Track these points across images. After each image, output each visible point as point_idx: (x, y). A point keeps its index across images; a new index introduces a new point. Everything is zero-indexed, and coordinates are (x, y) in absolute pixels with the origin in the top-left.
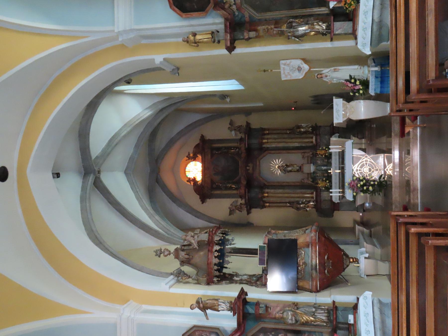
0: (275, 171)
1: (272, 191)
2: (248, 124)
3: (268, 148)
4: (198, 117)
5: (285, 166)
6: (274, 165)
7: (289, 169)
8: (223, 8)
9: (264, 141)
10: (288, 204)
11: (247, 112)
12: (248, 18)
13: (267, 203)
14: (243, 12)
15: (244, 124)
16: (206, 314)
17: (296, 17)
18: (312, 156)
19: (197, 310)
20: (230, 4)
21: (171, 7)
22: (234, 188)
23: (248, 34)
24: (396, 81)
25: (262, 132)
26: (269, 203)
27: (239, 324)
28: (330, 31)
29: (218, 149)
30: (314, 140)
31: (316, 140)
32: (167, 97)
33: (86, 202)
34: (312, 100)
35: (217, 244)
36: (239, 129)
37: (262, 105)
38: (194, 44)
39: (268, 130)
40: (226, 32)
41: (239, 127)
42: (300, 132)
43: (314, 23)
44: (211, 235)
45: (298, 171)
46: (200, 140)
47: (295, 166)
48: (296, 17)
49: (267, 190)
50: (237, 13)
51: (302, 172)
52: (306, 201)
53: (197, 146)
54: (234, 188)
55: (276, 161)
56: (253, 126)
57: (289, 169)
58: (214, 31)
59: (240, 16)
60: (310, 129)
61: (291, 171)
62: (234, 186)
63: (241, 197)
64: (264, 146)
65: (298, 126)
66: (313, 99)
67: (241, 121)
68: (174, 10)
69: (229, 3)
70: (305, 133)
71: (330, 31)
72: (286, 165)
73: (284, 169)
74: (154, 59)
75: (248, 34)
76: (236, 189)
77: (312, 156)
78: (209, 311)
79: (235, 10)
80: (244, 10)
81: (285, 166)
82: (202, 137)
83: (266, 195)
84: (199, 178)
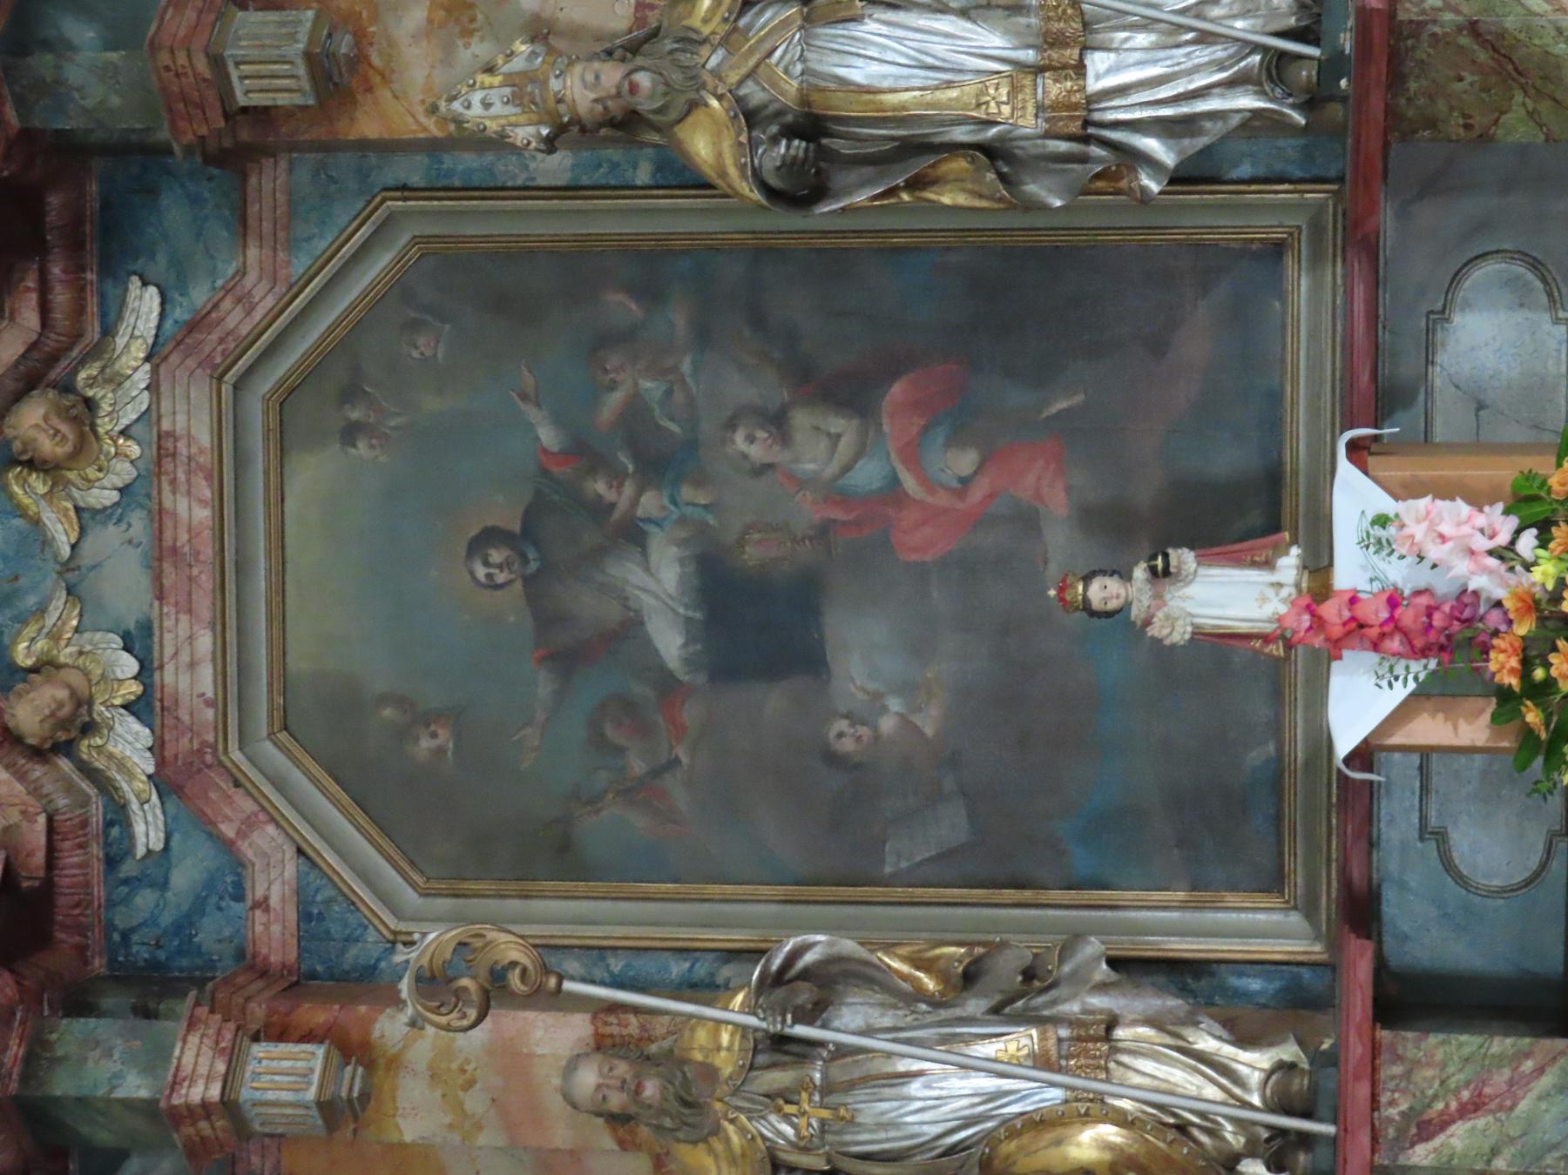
12: (292, 916)
14: (228, 830)
20: (82, 702)
23: (234, 1060)
24: (217, 547)
28: (1328, 1129)
50: (148, 831)
59: (185, 877)
69: (75, 678)
71: (1328, 1129)
75: (234, 1060)
79: (141, 784)
80: (249, 806)
84: (929, 731)
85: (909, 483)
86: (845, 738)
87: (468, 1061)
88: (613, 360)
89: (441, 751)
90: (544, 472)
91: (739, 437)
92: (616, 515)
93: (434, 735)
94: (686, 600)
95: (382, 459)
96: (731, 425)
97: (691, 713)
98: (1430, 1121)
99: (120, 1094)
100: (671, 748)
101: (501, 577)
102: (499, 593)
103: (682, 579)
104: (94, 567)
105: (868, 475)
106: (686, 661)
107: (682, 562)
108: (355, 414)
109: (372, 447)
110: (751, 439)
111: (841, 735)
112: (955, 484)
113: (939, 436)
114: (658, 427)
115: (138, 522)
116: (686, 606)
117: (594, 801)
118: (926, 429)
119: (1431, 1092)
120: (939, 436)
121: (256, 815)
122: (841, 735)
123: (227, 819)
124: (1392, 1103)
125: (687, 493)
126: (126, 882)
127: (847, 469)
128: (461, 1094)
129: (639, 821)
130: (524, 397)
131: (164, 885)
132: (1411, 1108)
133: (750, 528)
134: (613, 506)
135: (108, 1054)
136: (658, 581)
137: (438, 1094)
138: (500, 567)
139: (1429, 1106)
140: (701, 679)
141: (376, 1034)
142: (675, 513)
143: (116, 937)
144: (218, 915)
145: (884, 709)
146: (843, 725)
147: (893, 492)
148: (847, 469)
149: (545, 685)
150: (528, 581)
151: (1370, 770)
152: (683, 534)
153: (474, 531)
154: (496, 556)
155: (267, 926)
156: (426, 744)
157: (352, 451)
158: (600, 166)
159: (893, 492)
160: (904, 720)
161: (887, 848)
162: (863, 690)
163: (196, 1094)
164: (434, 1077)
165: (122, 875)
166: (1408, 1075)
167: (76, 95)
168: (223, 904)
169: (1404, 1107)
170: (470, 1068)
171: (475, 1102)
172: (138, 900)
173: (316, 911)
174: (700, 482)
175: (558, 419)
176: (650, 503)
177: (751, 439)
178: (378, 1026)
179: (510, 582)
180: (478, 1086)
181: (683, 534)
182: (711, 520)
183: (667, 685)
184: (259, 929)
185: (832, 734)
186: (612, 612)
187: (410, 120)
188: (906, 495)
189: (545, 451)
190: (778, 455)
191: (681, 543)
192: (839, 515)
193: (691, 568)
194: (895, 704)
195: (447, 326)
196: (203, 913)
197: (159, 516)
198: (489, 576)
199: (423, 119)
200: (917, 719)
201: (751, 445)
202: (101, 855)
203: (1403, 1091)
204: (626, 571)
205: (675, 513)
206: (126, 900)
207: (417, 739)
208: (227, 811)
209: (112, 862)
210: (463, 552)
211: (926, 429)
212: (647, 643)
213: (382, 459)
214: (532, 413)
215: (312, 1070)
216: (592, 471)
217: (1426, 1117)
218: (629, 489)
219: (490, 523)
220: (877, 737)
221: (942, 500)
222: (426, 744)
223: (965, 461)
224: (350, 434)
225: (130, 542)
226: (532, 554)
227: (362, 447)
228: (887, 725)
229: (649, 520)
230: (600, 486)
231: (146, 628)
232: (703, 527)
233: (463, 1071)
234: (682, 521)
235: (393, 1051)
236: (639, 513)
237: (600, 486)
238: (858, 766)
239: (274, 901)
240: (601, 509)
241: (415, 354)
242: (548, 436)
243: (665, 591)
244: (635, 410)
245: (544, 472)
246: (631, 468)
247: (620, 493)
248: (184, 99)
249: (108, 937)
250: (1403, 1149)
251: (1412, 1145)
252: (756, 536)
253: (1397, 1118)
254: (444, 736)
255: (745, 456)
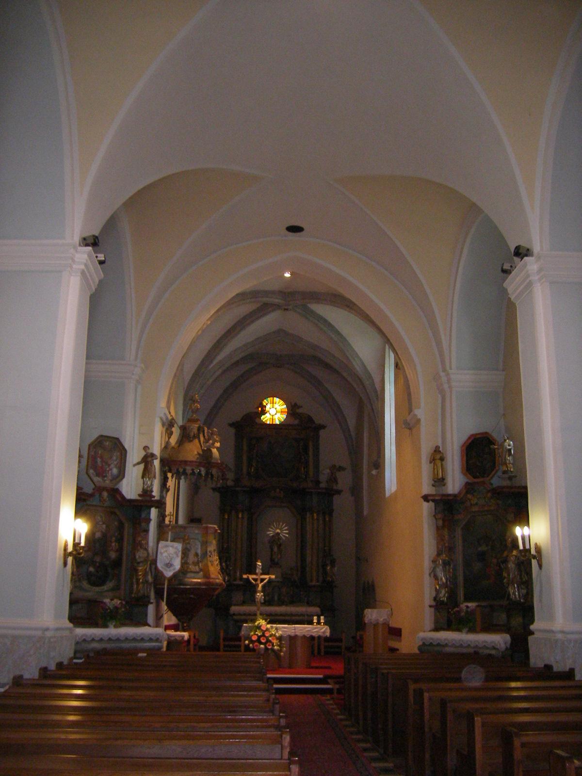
0: (272, 528)
1: (245, 524)
2: (339, 492)
3: (305, 519)
4: (352, 422)
5: (279, 543)
6: (281, 526)
7: (276, 549)
8: (467, 493)
9: (315, 515)
10: (227, 545)
11: (356, 490)
13: (229, 516)
15: (339, 487)
16: (138, 463)
17: (455, 569)
18: (292, 580)
19: (143, 454)
21: (472, 435)
22: (250, 470)
25: (328, 511)
26: (228, 518)
27: (131, 501)
29: (306, 449)
30: (314, 583)
31: (314, 586)
32: (379, 393)
33: (251, 298)
34: (368, 582)
35: (207, 472)
36: (333, 479)
37: (365, 513)
38: (432, 458)
39: (330, 521)
40: (444, 495)
41: (335, 479)
42: (327, 565)
43: (448, 588)
44: (216, 465)
45: (272, 560)
46: (320, 425)
47: (279, 556)
48: (455, 569)
49: (246, 516)
51: (271, 567)
52: (230, 570)
53: (310, 419)
54: (250, 470)
55: (285, 530)
56: (336, 498)
57: (276, 549)
58: (445, 481)
60: (329, 579)
61: (272, 550)
62: (252, 470)
63: (237, 480)
64: (308, 515)
65: (334, 562)
66: (370, 582)
67: (344, 480)
68: (469, 438)
70: (325, 573)
72: (280, 545)
73: (275, 540)
74: (419, 408)
76: (249, 474)
77: (292, 580)
78: (142, 466)
81: (279, 543)
82: (323, 427)
83: (240, 516)
84: (266, 418)
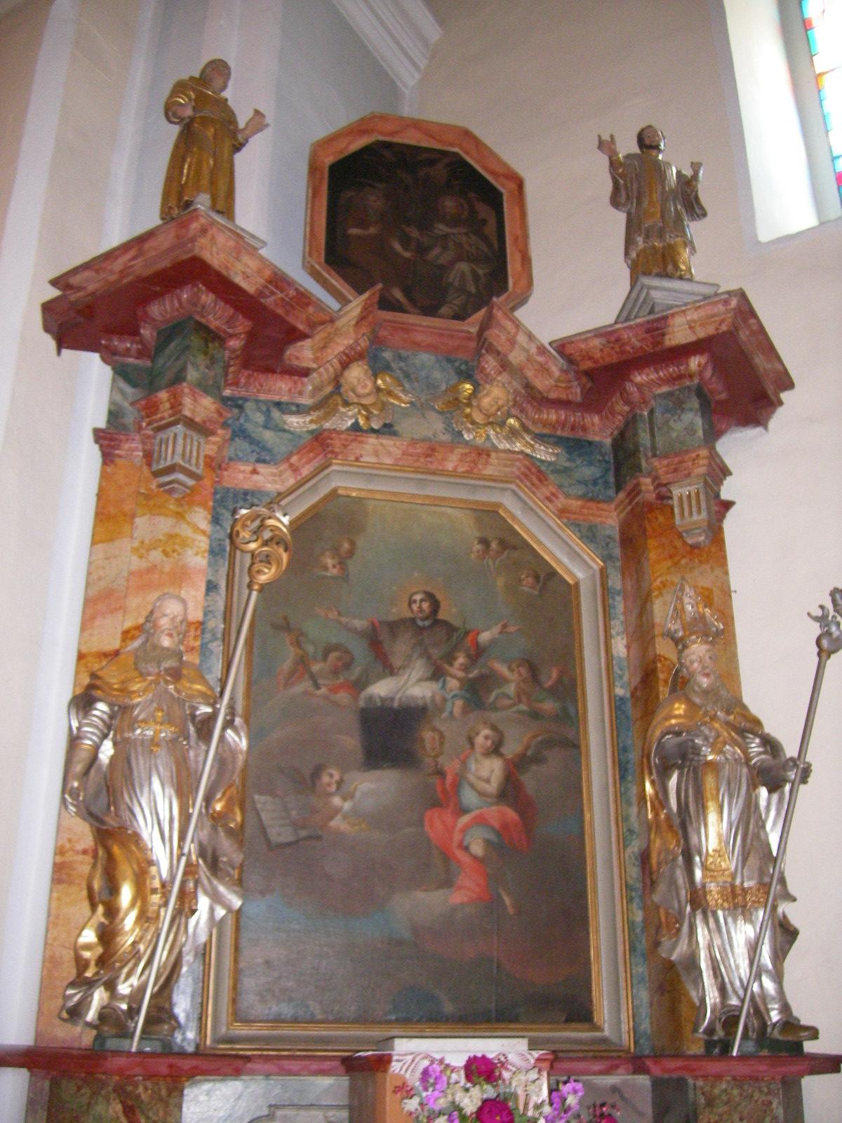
84: (333, 823)
85: (465, 819)
86: (330, 777)
87: (179, 554)
88: (523, 671)
89: (326, 569)
90: (467, 633)
91: (486, 732)
92: (446, 666)
93: (334, 567)
94: (404, 699)
95: (473, 556)
96: (494, 728)
97: (343, 697)
98: (134, 1114)
99: (190, 367)
100: (325, 686)
101: (415, 607)
102: (406, 604)
103: (414, 698)
104: (423, 415)
105: (469, 797)
106: (371, 698)
107: (423, 698)
108: (494, 545)
109: (478, 551)
110: (487, 738)
111: (331, 776)
112: (465, 844)
113: (491, 836)
114: (491, 692)
115: (446, 438)
116: (400, 699)
117: (298, 644)
118: (492, 828)
119: (150, 1114)
120: (491, 836)
121: (300, 475)
122: (331, 776)
123: (300, 460)
124: (146, 1089)
125: (459, 703)
126: (268, 410)
127: (472, 786)
128: (160, 549)
129: (287, 665)
130: (505, 626)
131: (266, 427)
132: (142, 1102)
133: (442, 736)
134: (451, 665)
135: (207, 367)
136: (413, 686)
137: (161, 537)
138: (420, 607)
139: (143, 1113)
140: (362, 704)
141: (197, 509)
142: (449, 696)
143: (240, 402)
144: (249, 450)
145: (344, 799)
146: (337, 777)
147: (462, 811)
148: (472, 786)
149: (359, 624)
150: (413, 620)
151: (738, 1017)
152: (438, 699)
153: (439, 596)
154: (425, 606)
155: (244, 472)
156: (330, 562)
157: (476, 542)
158: (621, 670)
159: (462, 811)
160: (337, 811)
161: (268, 797)
162: (355, 789)
163: (187, 401)
164: (171, 537)
165: (271, 408)
166: (161, 1100)
167: (676, 417)
168: (255, 454)
169: (144, 1097)
170: (175, 555)
171: (156, 556)
172: (258, 414)
173: (249, 498)
174: (465, 711)
175: (493, 642)
176: (453, 684)
177: (487, 738)
178: (201, 510)
179: (412, 611)
180: (164, 558)
181: (438, 699)
182: (445, 715)
183: (359, 686)
184: (242, 468)
185: (332, 771)
186: (396, 662)
187: (659, 573)
188: (460, 817)
189: (478, 634)
190: (478, 749)
191: (433, 698)
192: (449, 778)
193: (420, 703)
194: (347, 806)
195: (536, 593)
196: (251, 443)
197: (451, 447)
198: (415, 601)
199: (659, 580)
200: (339, 817)
201: (483, 737)
202: (282, 400)
203: (152, 1097)
204: (419, 669)
205: (449, 696)
206: (259, 409)
207: (333, 558)
208: (304, 460)
209: (278, 405)
210: (429, 589)
211: (492, 828)
212: (380, 677)
213: (473, 556)
214: (496, 630)
215: (190, 465)
216: (468, 656)
217: (137, 1112)
218: (461, 674)
219: (442, 604)
220: (331, 795)
221: (457, 837)
222: (330, 562)
223: (478, 849)
224: (485, 542)
225: (436, 433)
226: (427, 623)
227: (478, 547)
228: (336, 801)
229: (444, 682)
230: (461, 659)
231: (395, 434)
232: (441, 711)
233: (174, 551)
234: (445, 700)
235: (187, 516)
236: (448, 679)
237: (461, 659)
238: (314, 784)
239: (255, 477)
240: (450, 658)
241: (523, 576)
242: (485, 637)
243: (407, 689)
244: (502, 681)
245: (467, 633)
246: (471, 676)
247: (459, 669)
248: (681, 462)
249: (241, 398)
250: (119, 1096)
251: (122, 1102)
252: (437, 737)
253: (137, 1092)
254: (334, 572)
255: (477, 734)
